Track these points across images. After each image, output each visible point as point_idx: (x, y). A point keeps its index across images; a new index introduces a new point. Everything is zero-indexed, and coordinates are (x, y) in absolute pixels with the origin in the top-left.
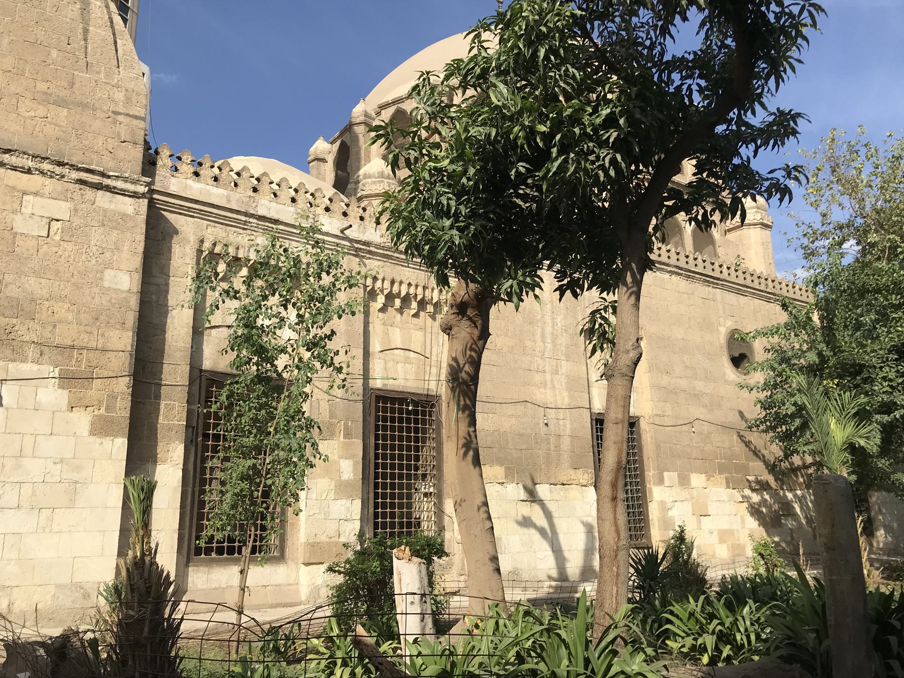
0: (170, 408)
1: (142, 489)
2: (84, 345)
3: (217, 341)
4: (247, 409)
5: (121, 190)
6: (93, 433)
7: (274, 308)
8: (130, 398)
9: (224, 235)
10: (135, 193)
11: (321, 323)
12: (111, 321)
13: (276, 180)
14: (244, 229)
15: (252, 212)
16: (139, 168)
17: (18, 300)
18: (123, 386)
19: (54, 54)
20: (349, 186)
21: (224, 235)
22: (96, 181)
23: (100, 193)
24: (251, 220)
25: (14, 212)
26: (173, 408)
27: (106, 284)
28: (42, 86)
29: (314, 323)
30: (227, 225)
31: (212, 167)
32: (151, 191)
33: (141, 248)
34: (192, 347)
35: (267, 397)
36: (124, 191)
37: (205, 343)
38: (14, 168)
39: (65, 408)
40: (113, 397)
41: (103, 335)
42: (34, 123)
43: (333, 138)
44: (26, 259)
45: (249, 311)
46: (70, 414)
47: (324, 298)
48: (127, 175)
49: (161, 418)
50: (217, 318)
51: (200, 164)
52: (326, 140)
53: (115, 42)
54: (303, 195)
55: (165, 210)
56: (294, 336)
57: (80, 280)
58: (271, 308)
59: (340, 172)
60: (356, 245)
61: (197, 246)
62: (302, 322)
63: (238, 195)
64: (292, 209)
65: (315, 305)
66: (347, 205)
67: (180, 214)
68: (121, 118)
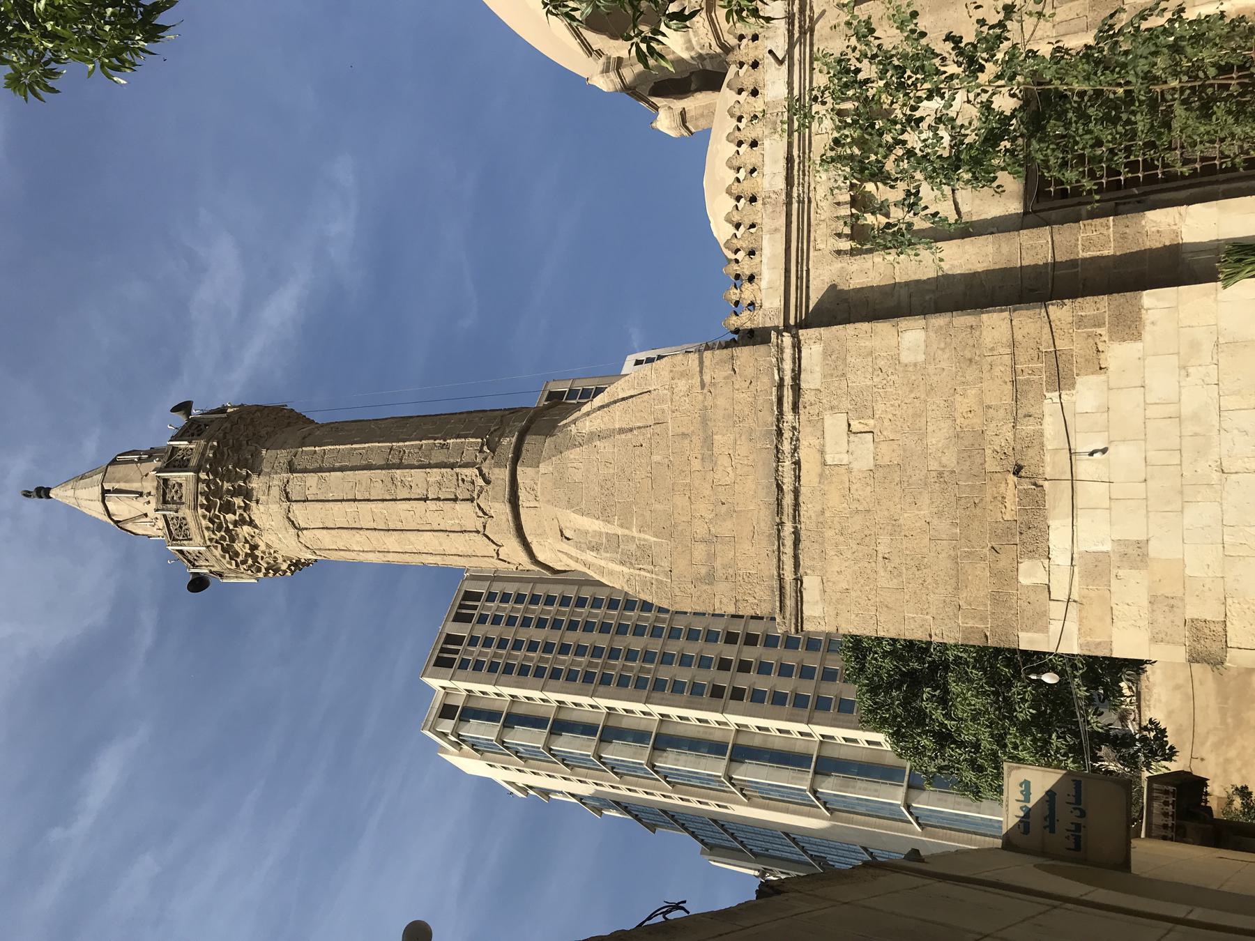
0: (1089, 243)
1: (1240, 261)
2: (1009, 369)
3: (977, 202)
4: (1088, 137)
5: (794, 363)
6: (1138, 337)
7: (923, 136)
8: (1080, 300)
9: (823, 225)
10: (794, 347)
11: (937, 61)
12: (971, 343)
13: (732, 175)
14: (810, 201)
15: (784, 196)
16: (762, 349)
17: (959, 452)
18: (1061, 312)
19: (656, 458)
20: (709, 68)
21: (823, 225)
22: (791, 391)
23: (803, 385)
24: (795, 195)
25: (850, 471)
26: (1089, 239)
27: (921, 358)
28: (696, 465)
29: (938, 72)
30: (809, 225)
31: (737, 261)
32: (787, 327)
33: (865, 326)
34: (992, 233)
35: (1066, 111)
36: (794, 359)
37: (983, 217)
38: (798, 478)
39: (1103, 377)
40: (1080, 322)
41: (992, 349)
42: (739, 466)
43: (650, 109)
44: (905, 450)
45: (934, 170)
46: (1111, 369)
47: (896, 67)
48: (774, 360)
49: (1106, 253)
50: (946, 210)
51: (738, 277)
52: (655, 117)
53: (623, 399)
54: (743, 132)
55: (807, 307)
56: (961, 96)
57: (922, 388)
58: (925, 140)
59: (693, 87)
60: (796, 35)
61: (847, 257)
62: (938, 90)
63: (766, 220)
64: (767, 143)
65: (910, 77)
66: (741, 64)
67: (808, 287)
68: (707, 379)
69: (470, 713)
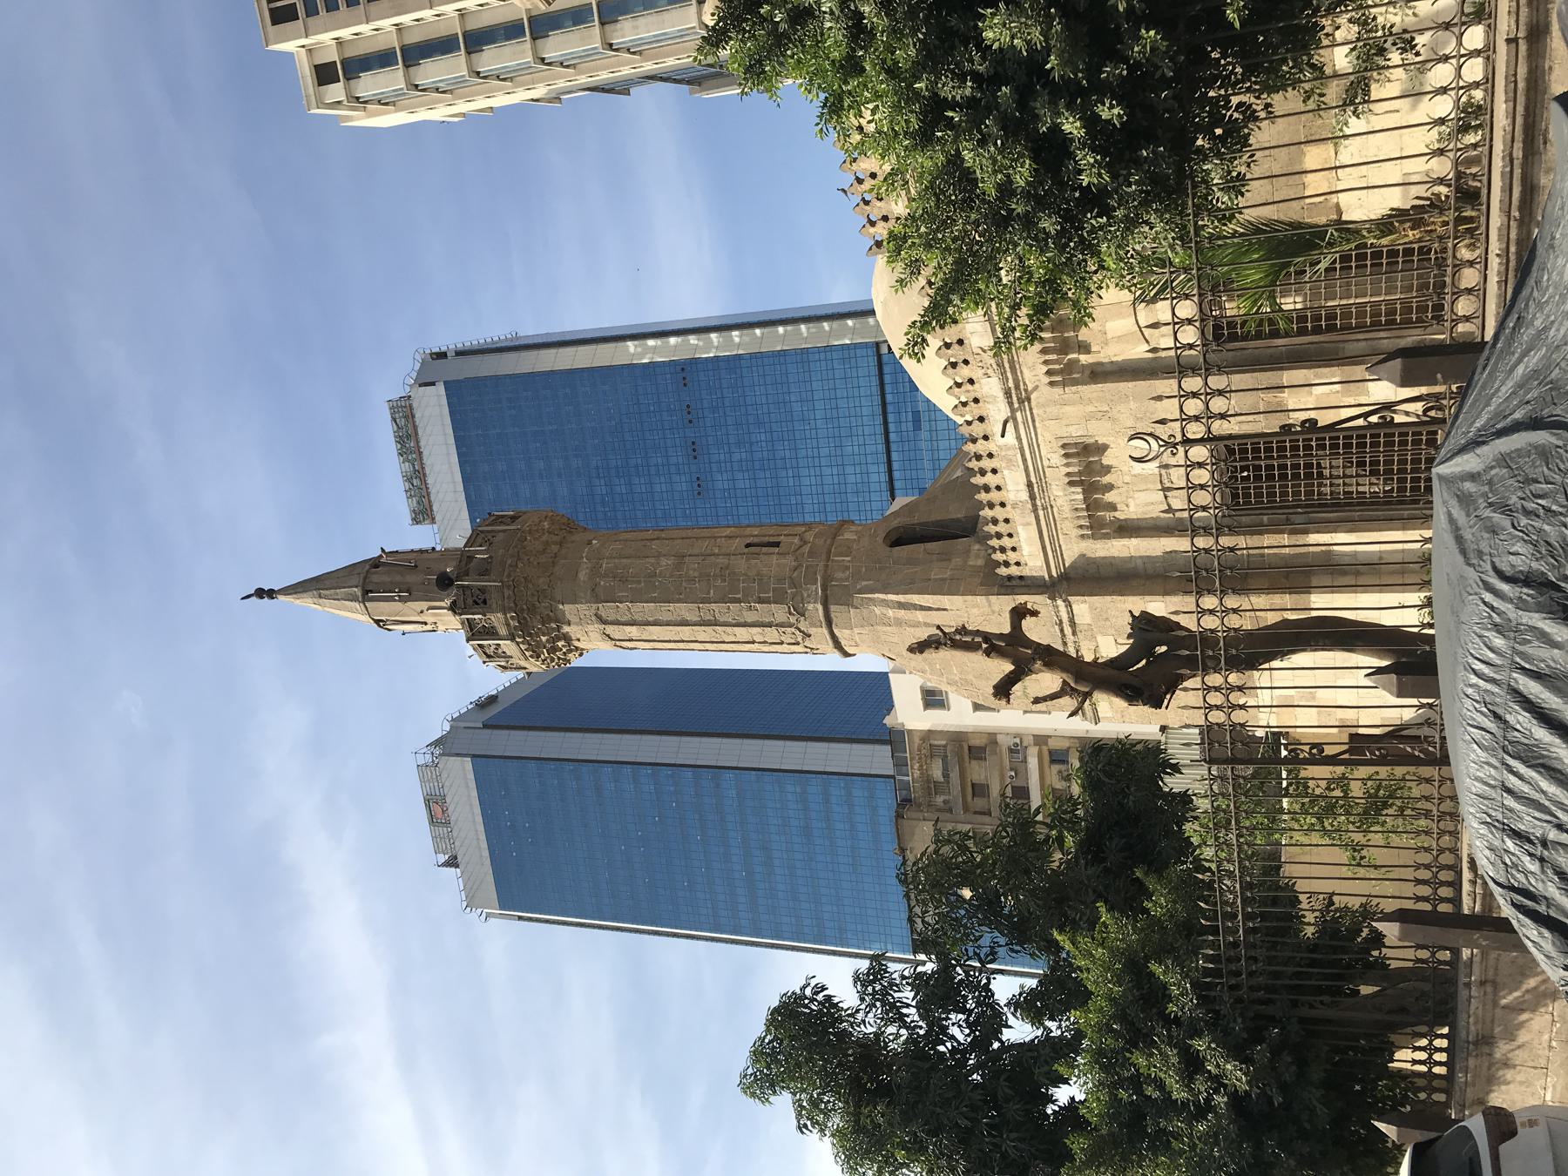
69: (356, 66)
